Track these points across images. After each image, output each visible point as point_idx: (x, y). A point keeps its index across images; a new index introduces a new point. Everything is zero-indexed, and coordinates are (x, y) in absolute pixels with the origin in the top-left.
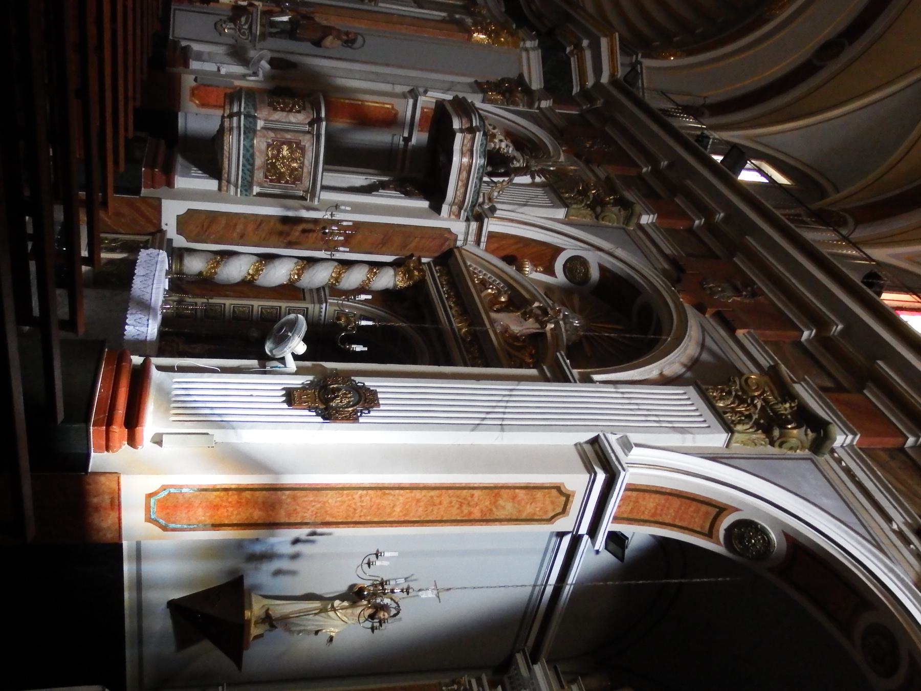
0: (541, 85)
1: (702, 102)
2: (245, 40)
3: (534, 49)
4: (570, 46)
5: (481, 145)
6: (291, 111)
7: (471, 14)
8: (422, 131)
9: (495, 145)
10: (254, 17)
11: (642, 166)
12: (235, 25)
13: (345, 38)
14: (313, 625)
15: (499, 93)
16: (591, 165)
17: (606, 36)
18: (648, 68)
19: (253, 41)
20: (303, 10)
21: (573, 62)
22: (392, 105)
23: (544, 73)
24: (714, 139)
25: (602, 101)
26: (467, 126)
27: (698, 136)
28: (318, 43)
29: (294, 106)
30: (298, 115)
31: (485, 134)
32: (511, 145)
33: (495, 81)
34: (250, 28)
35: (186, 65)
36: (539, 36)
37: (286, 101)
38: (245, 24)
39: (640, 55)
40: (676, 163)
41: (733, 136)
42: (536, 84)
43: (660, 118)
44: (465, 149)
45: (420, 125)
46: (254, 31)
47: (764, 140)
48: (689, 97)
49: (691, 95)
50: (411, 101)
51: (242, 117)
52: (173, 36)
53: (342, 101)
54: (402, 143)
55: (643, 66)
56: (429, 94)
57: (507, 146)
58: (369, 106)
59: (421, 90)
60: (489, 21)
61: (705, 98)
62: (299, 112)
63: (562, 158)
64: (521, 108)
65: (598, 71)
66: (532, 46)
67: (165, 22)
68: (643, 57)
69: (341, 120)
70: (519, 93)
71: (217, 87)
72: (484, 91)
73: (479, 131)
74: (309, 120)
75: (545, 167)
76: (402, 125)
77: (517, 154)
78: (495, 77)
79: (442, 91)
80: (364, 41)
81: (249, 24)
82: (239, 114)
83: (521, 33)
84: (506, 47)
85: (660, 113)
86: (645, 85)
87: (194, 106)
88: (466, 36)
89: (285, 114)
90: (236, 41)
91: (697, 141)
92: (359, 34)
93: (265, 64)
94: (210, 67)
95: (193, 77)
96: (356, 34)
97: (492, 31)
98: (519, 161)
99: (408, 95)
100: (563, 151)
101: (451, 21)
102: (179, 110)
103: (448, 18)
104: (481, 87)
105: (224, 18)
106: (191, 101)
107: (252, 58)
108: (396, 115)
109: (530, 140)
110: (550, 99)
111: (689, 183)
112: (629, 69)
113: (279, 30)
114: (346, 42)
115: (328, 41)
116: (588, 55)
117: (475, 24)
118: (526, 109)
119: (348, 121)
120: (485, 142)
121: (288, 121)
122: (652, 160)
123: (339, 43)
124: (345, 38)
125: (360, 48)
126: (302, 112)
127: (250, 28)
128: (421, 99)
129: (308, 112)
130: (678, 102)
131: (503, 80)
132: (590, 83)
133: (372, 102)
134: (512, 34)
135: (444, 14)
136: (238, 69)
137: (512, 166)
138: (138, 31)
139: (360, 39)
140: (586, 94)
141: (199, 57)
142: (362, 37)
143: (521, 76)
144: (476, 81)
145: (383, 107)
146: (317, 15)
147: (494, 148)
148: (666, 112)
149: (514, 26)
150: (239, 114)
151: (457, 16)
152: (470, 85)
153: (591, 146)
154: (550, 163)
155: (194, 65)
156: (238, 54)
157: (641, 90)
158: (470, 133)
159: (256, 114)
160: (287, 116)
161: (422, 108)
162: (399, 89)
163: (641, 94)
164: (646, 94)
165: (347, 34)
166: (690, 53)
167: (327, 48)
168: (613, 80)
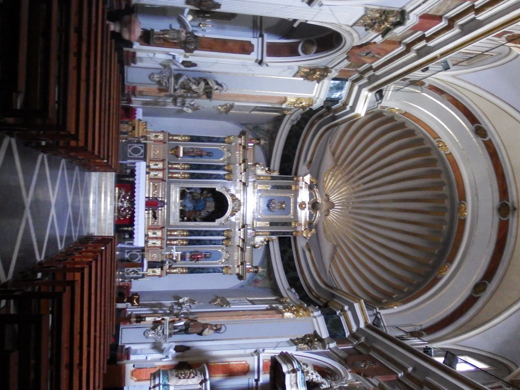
0: (327, 335)
1: (419, 328)
2: (160, 339)
3: (319, 316)
4: (338, 311)
5: (302, 378)
6: (189, 378)
7: (281, 303)
8: (265, 373)
9: (310, 377)
10: (165, 326)
11: (398, 373)
12: (155, 331)
13: (215, 328)
14: (110, 331)
15: (305, 344)
16: (368, 378)
17: (357, 302)
18: (383, 315)
19: (165, 339)
20: (191, 317)
21: (342, 319)
22: (246, 361)
23: (328, 328)
24: (434, 348)
25: (364, 338)
26: (292, 368)
27: (424, 349)
28: (200, 334)
29: (190, 374)
30: (193, 379)
31: (303, 372)
32: (318, 375)
33: (302, 337)
34: (163, 332)
35: (128, 358)
36: (320, 307)
37: (186, 372)
38: (160, 330)
39: (378, 309)
40: (417, 367)
41: (444, 345)
42: (324, 334)
43: (398, 342)
44: (292, 383)
45: (263, 370)
46: (165, 333)
47: (462, 343)
48: (411, 327)
49: (411, 326)
50: (256, 357)
51: (161, 386)
52: (121, 343)
53: (217, 364)
54: (254, 383)
55: (381, 314)
56: (266, 351)
57: (317, 376)
58: (232, 364)
59: (261, 350)
60: (291, 305)
61: (420, 325)
62: (193, 377)
63: (350, 377)
64: (319, 350)
65: (357, 322)
66: (318, 314)
67: (117, 337)
68: (380, 309)
69: (218, 375)
70: (316, 341)
71: (146, 368)
72: (296, 344)
73: (299, 371)
74: (200, 381)
75: (342, 385)
76: (253, 372)
77: (323, 380)
78: (301, 336)
79: (273, 348)
80: (226, 328)
81: (162, 329)
82: (159, 385)
83: (310, 309)
84: (303, 318)
85: (398, 339)
86: (386, 325)
87: (133, 381)
88: (281, 315)
89: (185, 380)
90: (156, 340)
91: (424, 352)
92: (222, 325)
93: (172, 352)
94: (142, 357)
95: (132, 365)
96: (221, 325)
97: (295, 310)
98: (325, 384)
99: (254, 354)
100: (349, 372)
101: (272, 309)
102: (124, 386)
103: (269, 308)
104: (294, 342)
105: (149, 329)
106: (132, 379)
107: (165, 348)
108: (248, 367)
109: (328, 369)
110: (334, 342)
111: (429, 379)
112: (374, 317)
113: (179, 330)
114: (216, 330)
115: (206, 332)
116: (349, 314)
117: (285, 308)
118: (322, 350)
119: (221, 375)
120: (303, 376)
121: (187, 384)
122: (403, 369)
123: (212, 331)
124: (215, 328)
125: (224, 332)
126: (195, 377)
127: (163, 332)
128: (262, 356)
129: (199, 377)
130: (407, 331)
131: (306, 336)
132: (354, 329)
133: (235, 362)
134: (305, 310)
135: (267, 306)
136: (159, 356)
137: (322, 388)
138: (102, 347)
139: (223, 327)
140: (354, 336)
141: (136, 353)
142: (226, 328)
143: (315, 332)
144: (291, 339)
145: (241, 364)
146: (199, 318)
147: (309, 379)
148: (401, 338)
149: (306, 305)
150: (159, 385)
151: (274, 305)
152: (288, 342)
153: (365, 367)
154: (344, 382)
155: (133, 358)
156: (157, 347)
157: (384, 328)
158: (294, 373)
159: (169, 383)
160: (187, 381)
161: (263, 360)
162: (249, 351)
163: (384, 330)
164: (387, 330)
165: (216, 326)
166: (404, 303)
167: (206, 335)
168: (368, 326)
